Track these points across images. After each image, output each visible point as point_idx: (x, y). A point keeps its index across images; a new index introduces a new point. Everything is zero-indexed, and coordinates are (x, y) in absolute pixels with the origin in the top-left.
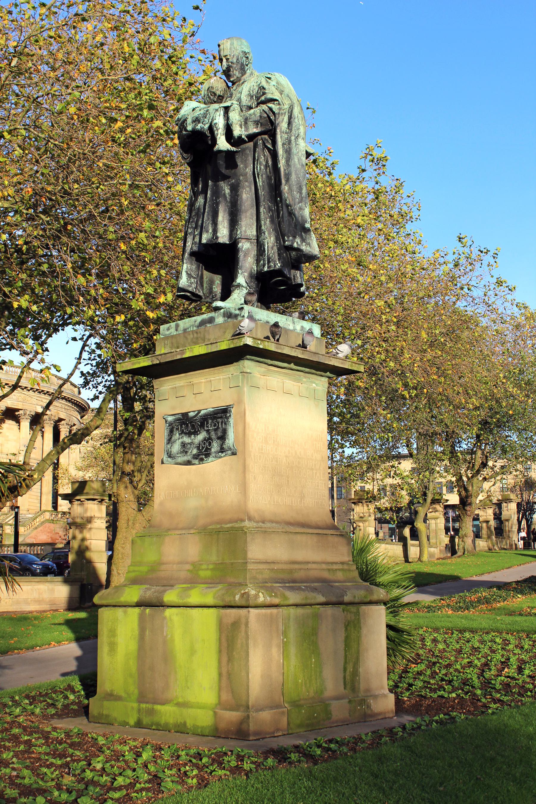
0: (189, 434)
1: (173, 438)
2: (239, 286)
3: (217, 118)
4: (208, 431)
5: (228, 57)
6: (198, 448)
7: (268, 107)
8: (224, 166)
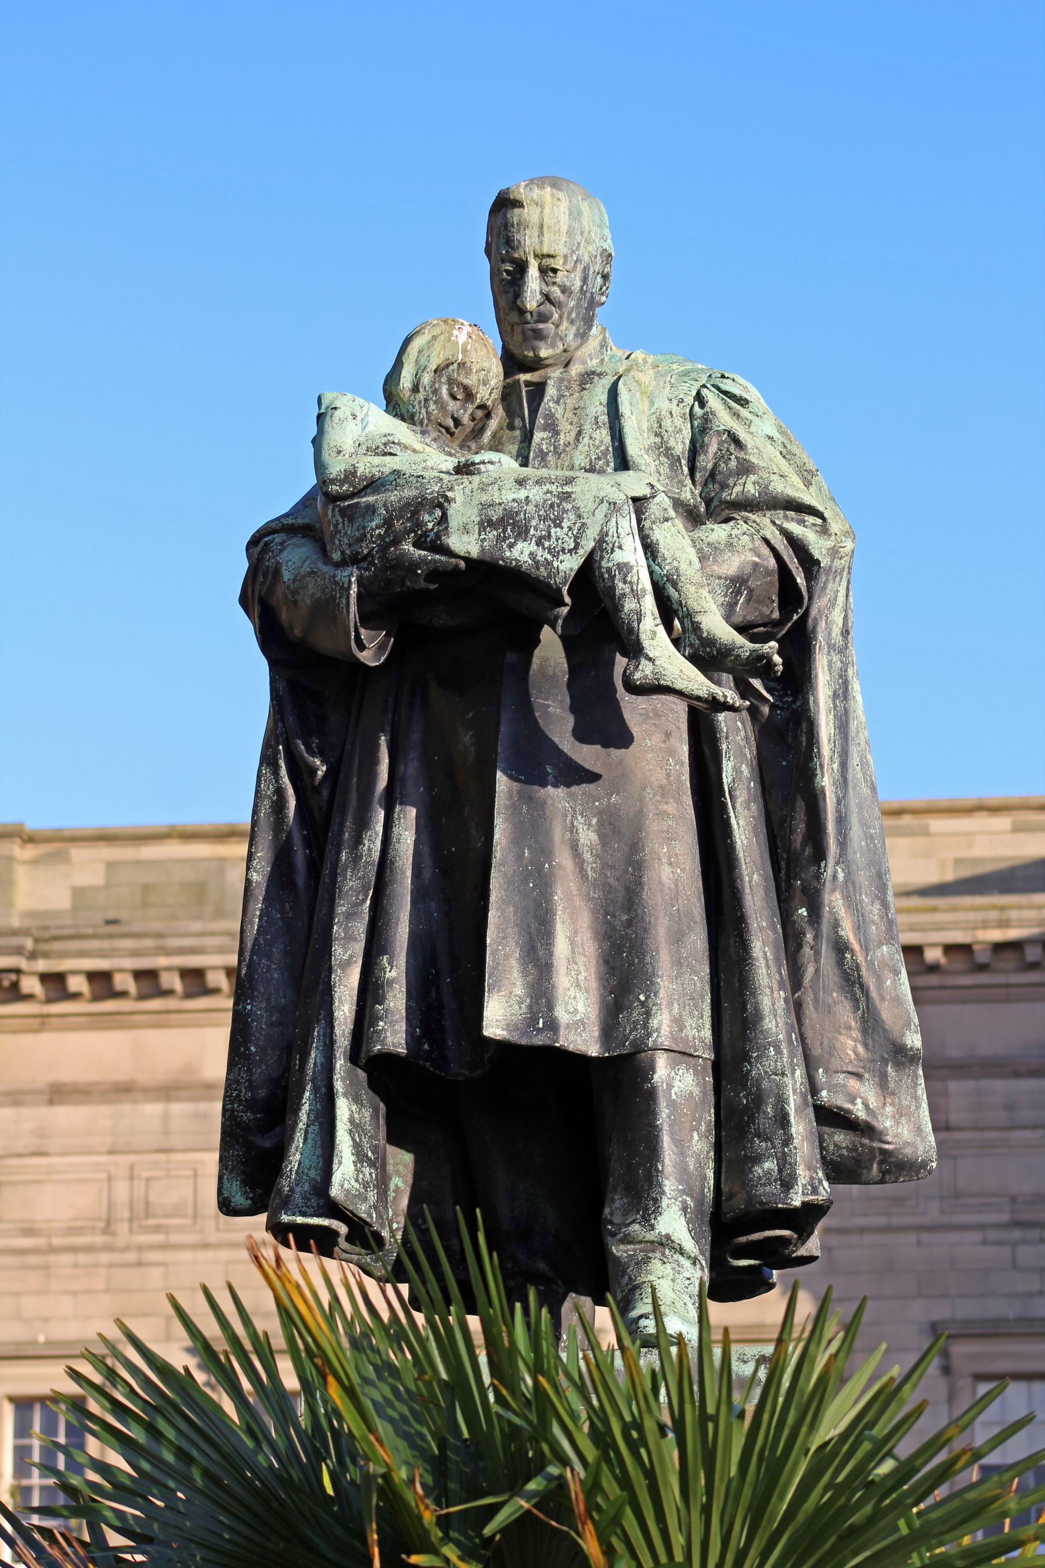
5: (558, 263)
8: (570, 721)
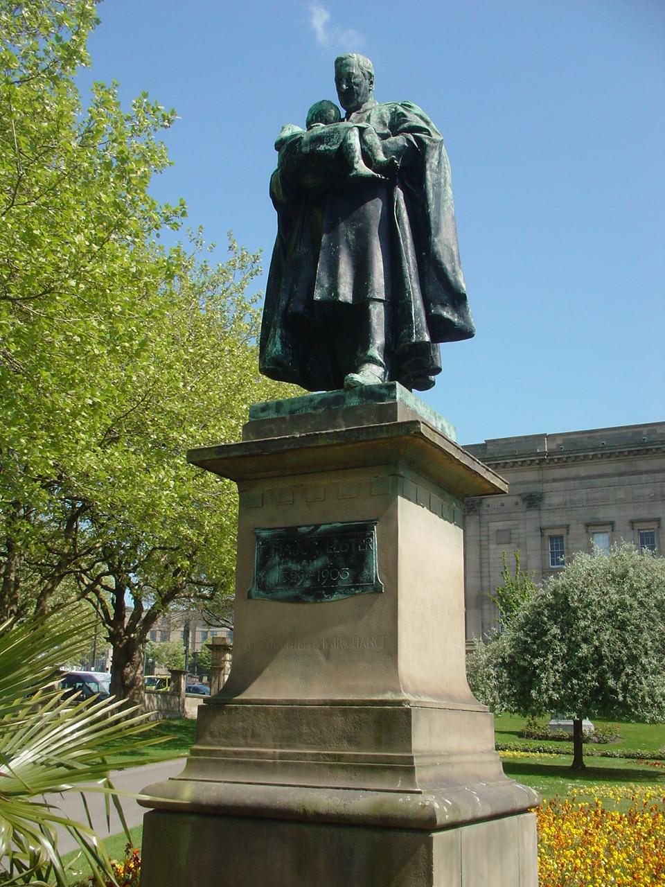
2: (372, 360)
4: (331, 556)
6: (314, 579)
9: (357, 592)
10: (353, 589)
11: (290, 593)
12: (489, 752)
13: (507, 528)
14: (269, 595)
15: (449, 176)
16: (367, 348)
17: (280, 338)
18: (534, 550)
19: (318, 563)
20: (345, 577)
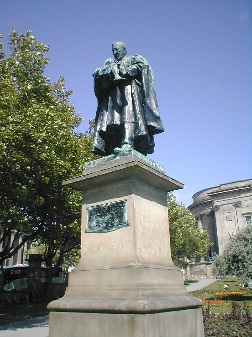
0: (101, 216)
1: (92, 219)
2: (126, 143)
3: (115, 68)
6: (106, 223)
7: (138, 65)
9: (121, 226)
10: (119, 225)
11: (99, 229)
12: (181, 285)
13: (230, 215)
14: (92, 230)
15: (152, 77)
16: (124, 139)
17: (97, 140)
18: (241, 222)
19: (108, 217)
20: (117, 221)
